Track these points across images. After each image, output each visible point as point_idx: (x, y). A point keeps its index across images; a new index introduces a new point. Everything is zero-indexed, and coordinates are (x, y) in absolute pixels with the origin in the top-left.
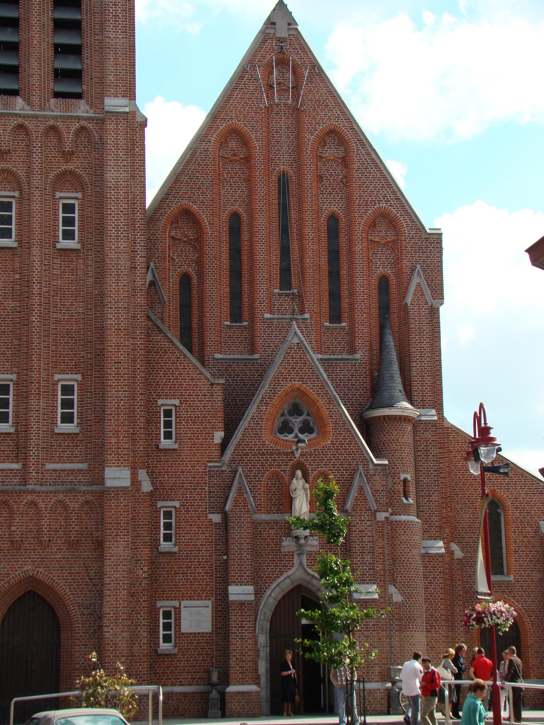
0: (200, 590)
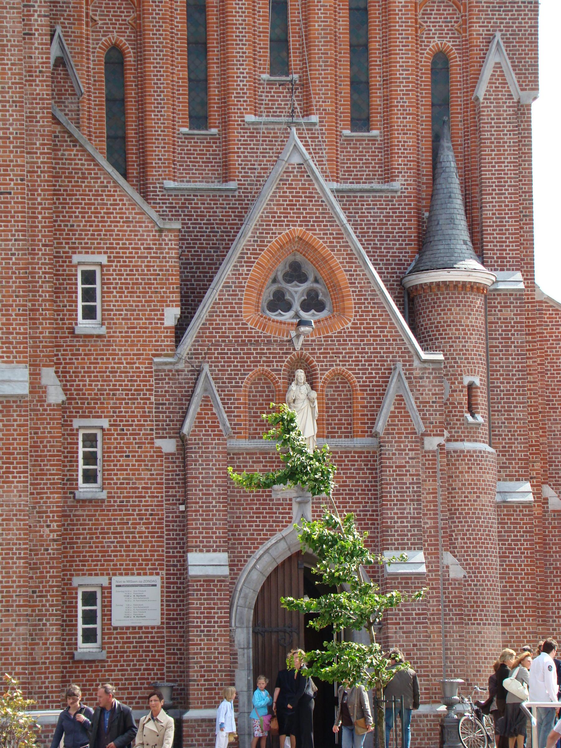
0: (143, 560)
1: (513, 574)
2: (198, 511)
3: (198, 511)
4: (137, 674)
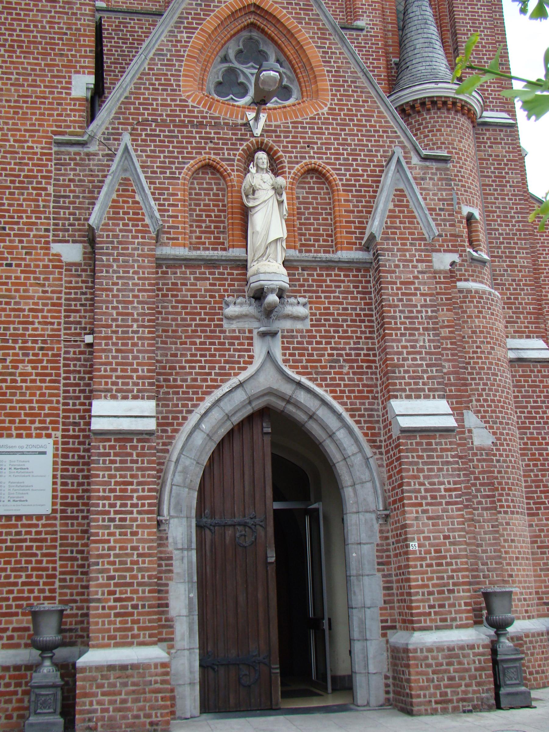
0: (26, 415)
1: (536, 449)
2: (111, 338)
3: (111, 338)
4: (11, 592)
